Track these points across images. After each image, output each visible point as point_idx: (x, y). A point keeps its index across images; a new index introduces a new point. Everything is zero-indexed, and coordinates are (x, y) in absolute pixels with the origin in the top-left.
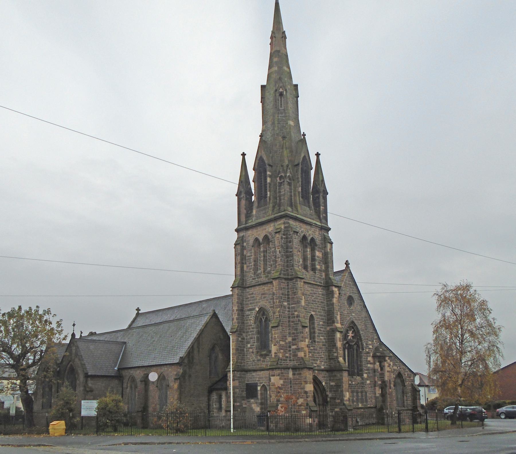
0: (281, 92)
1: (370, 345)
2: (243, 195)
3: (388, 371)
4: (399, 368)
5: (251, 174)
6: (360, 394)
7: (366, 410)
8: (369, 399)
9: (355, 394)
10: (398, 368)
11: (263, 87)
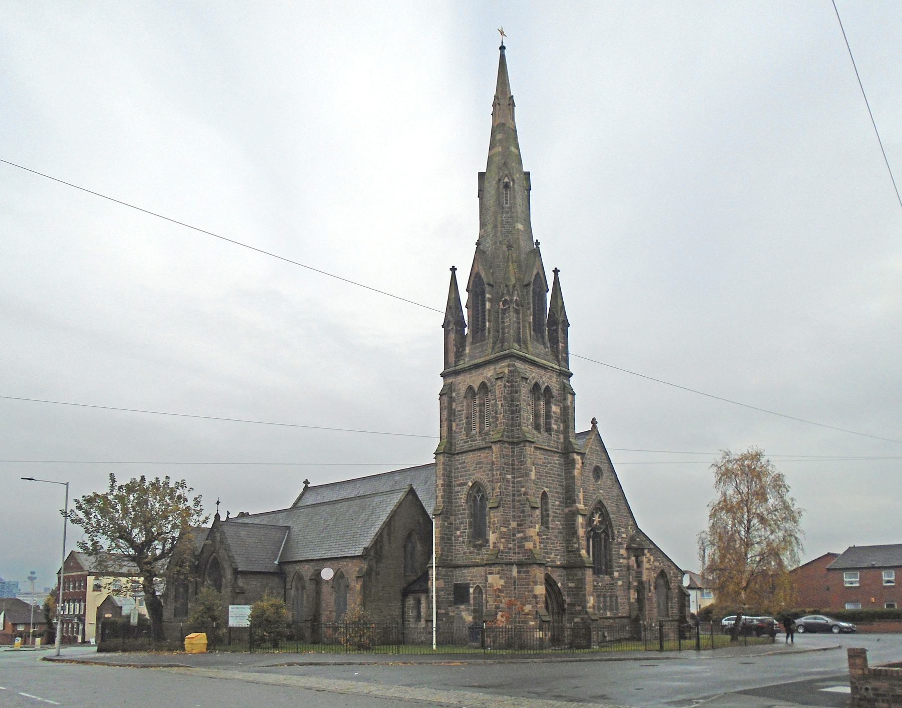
0: (507, 182)
2: (452, 326)
4: (662, 564)
5: (464, 297)
6: (608, 599)
9: (602, 599)
10: (660, 564)
11: (481, 175)
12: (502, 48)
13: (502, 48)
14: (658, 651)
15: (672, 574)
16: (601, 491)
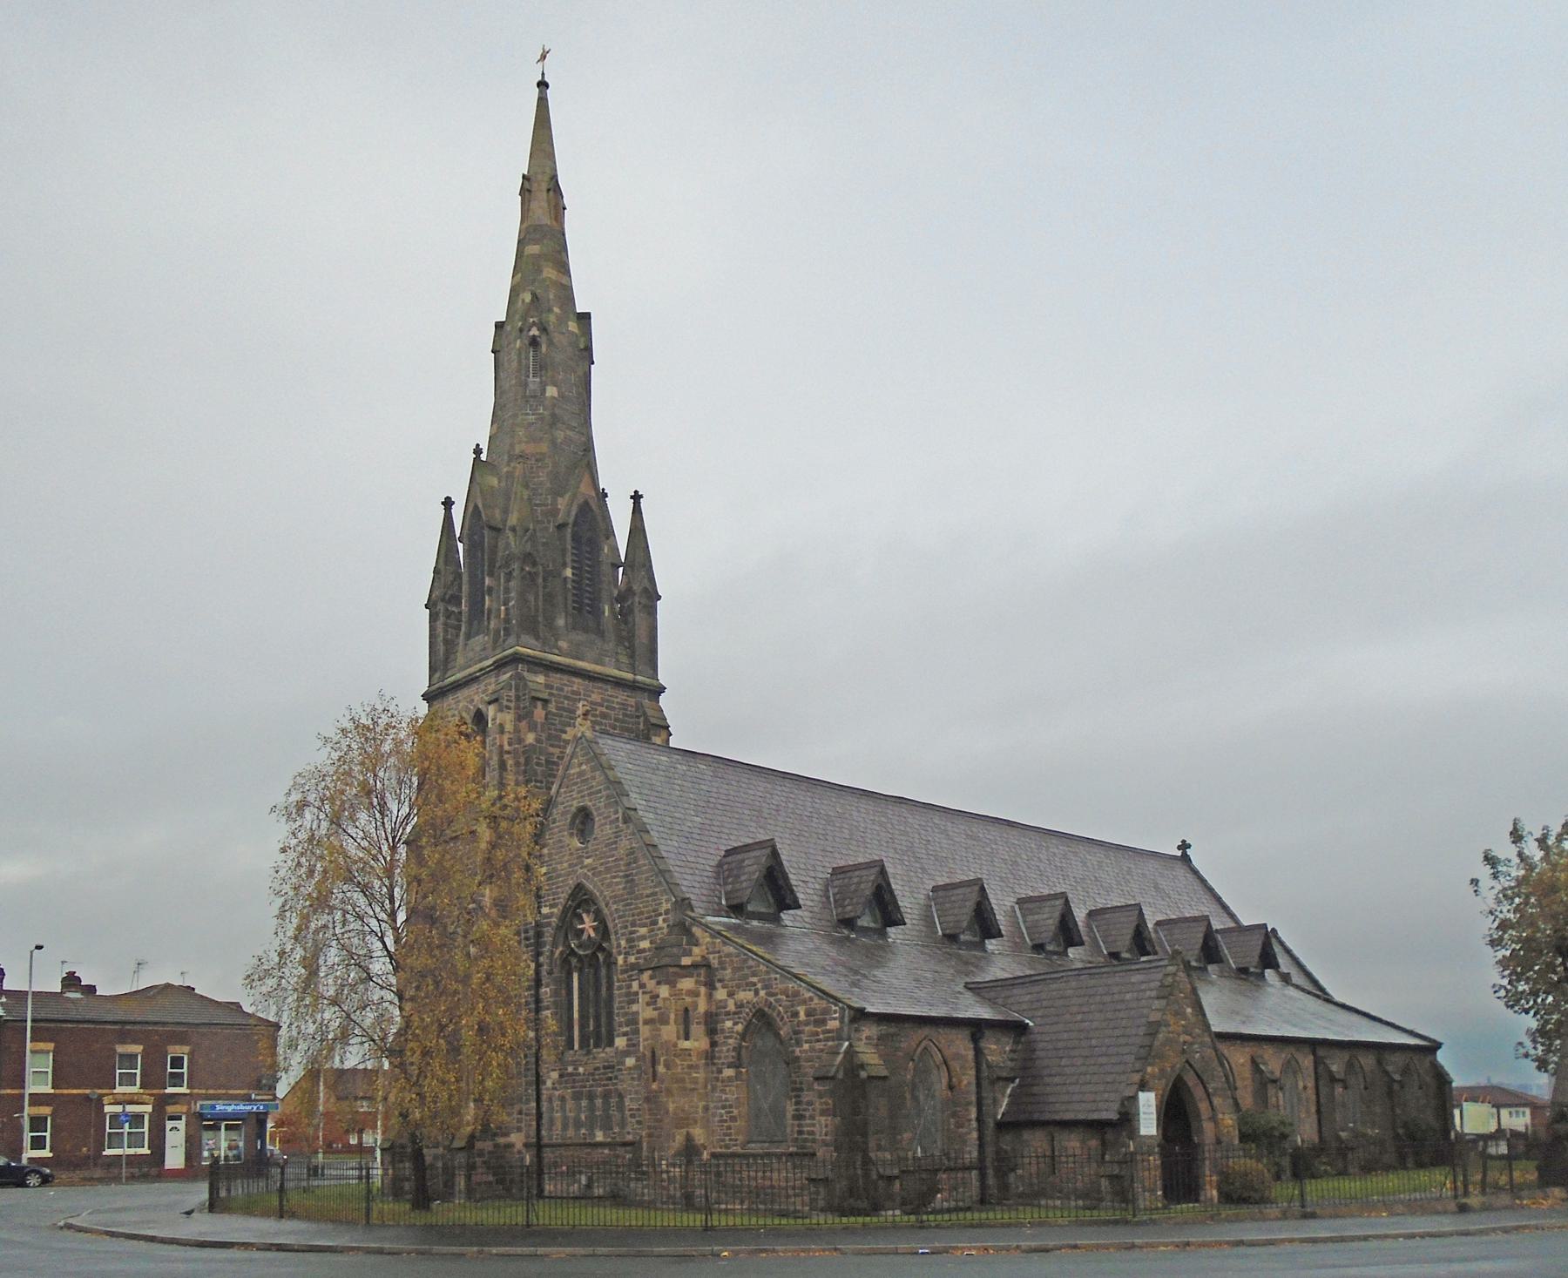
1: (643, 938)
3: (646, 1022)
4: (762, 993)
6: (599, 1102)
7: (620, 1151)
8: (632, 1116)
9: (584, 1103)
10: (757, 993)
11: (499, 326)
12: (543, 85)
13: (543, 85)
14: (1280, 1219)
15: (802, 1017)
16: (589, 861)
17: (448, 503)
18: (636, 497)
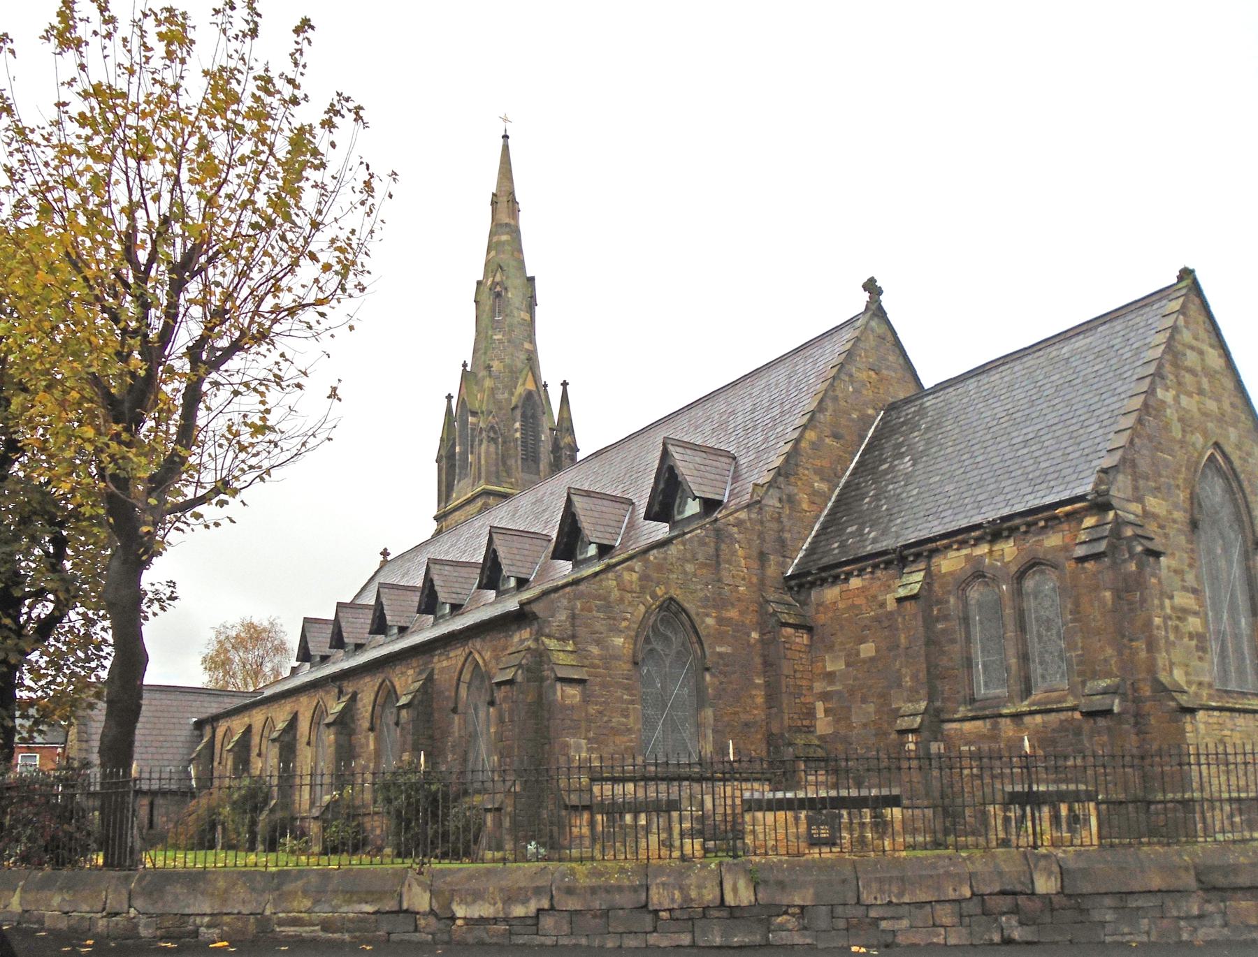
11: (479, 283)
12: (506, 137)
13: (506, 137)
17: (449, 397)
18: (565, 384)
